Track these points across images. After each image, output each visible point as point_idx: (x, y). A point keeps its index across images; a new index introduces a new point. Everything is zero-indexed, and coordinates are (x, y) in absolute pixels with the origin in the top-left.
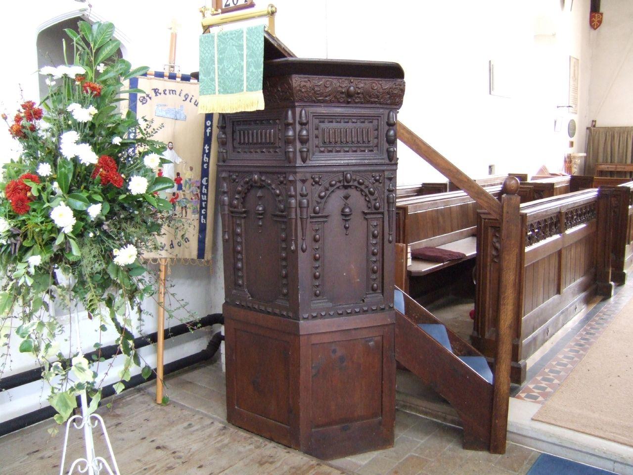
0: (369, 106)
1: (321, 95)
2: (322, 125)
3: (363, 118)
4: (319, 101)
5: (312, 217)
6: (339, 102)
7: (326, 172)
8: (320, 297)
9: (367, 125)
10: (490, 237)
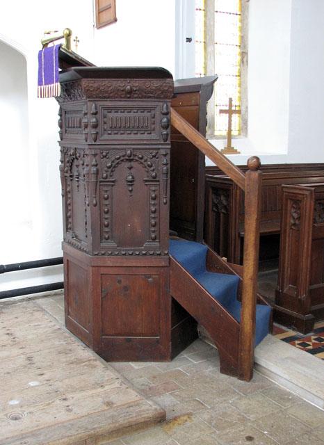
0: (146, 99)
1: (106, 92)
2: (110, 115)
3: (143, 109)
4: (105, 97)
5: (101, 182)
6: (121, 98)
7: (114, 149)
8: (109, 241)
9: (146, 114)
10: (289, 209)
